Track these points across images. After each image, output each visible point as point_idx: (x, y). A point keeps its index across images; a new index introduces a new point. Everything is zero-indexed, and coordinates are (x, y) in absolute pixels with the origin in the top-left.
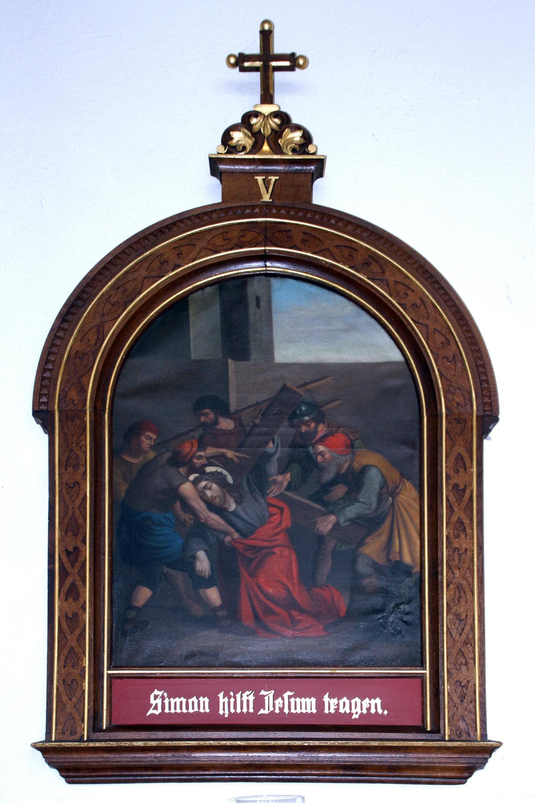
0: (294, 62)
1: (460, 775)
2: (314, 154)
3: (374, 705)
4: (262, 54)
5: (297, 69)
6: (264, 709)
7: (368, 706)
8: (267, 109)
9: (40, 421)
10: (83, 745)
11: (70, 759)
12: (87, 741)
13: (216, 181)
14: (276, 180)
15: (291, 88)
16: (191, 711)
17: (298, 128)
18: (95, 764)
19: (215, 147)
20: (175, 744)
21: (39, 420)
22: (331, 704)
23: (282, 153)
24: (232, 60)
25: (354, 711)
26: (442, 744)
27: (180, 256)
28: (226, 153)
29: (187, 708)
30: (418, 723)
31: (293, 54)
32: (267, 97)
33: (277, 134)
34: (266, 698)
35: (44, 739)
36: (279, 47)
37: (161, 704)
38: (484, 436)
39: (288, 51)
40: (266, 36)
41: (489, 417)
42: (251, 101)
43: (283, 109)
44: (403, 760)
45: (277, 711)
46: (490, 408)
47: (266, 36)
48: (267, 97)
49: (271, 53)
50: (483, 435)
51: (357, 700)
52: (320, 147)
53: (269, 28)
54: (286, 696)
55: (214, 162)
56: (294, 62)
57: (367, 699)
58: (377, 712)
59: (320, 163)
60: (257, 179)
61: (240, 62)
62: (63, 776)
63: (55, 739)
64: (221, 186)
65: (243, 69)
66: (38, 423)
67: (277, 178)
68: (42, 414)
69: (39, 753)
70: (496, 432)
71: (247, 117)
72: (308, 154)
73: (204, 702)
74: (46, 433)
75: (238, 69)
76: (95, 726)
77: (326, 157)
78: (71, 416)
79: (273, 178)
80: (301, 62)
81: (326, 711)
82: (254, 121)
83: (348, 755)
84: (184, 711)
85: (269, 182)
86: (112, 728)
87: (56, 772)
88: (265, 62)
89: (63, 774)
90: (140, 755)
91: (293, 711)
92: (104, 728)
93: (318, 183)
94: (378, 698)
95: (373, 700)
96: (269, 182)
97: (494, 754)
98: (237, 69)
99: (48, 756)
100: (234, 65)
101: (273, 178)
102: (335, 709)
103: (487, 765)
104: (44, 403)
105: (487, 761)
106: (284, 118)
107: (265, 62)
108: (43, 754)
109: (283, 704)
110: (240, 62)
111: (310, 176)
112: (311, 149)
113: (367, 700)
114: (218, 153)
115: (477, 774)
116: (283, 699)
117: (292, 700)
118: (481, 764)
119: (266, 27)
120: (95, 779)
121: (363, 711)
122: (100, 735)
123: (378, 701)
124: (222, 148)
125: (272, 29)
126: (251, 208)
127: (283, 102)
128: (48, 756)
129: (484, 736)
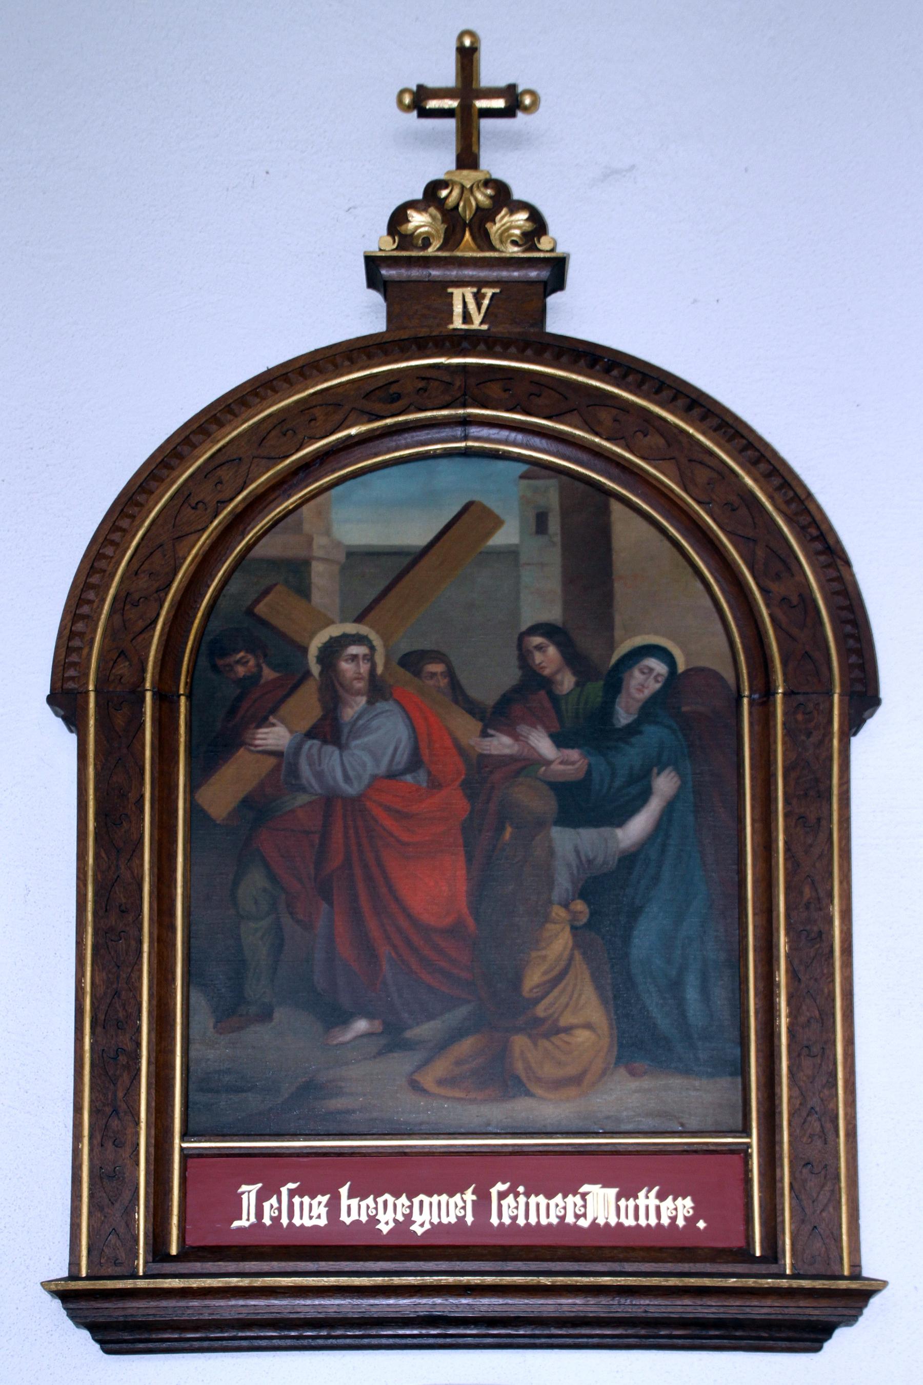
0: (515, 102)
1: (809, 1335)
2: (552, 250)
3: (663, 1210)
4: (460, 86)
5: (520, 114)
6: (240, 1218)
7: (408, 1211)
8: (468, 177)
9: (62, 713)
10: (784, 1283)
11: (107, 1310)
12: (88, 1278)
13: (376, 298)
14: (494, 294)
15: (516, 141)
16: (643, 1222)
17: (524, 206)
18: (572, 1315)
19: (379, 241)
20: (226, 1282)
21: (57, 709)
22: (354, 1210)
23: (493, 248)
24: (407, 99)
25: (416, 1216)
26: (129, 1284)
27: (313, 423)
28: (396, 249)
29: (637, 1217)
30: (737, 1242)
31: (512, 88)
32: (467, 158)
33: (485, 215)
34: (245, 1197)
35: (65, 1273)
36: (490, 74)
37: (254, 1208)
38: (854, 730)
39: (502, 83)
40: (467, 57)
41: (864, 698)
42: (442, 163)
43: (495, 176)
44: (689, 1309)
45: (267, 1221)
46: (861, 675)
47: (467, 57)
48: (467, 158)
49: (474, 86)
50: (850, 729)
51: (541, 1199)
52: (561, 237)
53: (472, 43)
54: (284, 1190)
55: (372, 263)
56: (515, 102)
57: (670, 1198)
58: (538, 1223)
59: (557, 269)
60: (452, 294)
61: (419, 101)
62: (97, 1341)
63: (144, 1272)
64: (384, 304)
65: (425, 113)
66: (57, 714)
67: (497, 290)
68: (64, 700)
69: (57, 1304)
70: (872, 725)
71: (433, 188)
72: (539, 250)
73: (538, 1205)
74: (71, 731)
75: (415, 113)
76: (158, 1251)
77: (569, 255)
78: (119, 703)
79: (489, 292)
80: (527, 101)
81: (495, 1221)
82: (444, 193)
83: (501, 1301)
84: (533, 1220)
85: (465, 311)
86: (186, 1254)
87: (85, 1334)
88: (467, 102)
89: (100, 1337)
90: (647, 1302)
91: (297, 1221)
92: (758, 1254)
93: (553, 300)
94: (689, 1198)
95: (631, 1200)
96: (465, 311)
97: (875, 1301)
98: (415, 113)
99: (71, 1306)
100: (408, 109)
101: (489, 292)
102: (670, 1218)
103: (861, 1319)
104: (72, 678)
105: (861, 1314)
106: (502, 195)
107: (467, 102)
108: (63, 1302)
109: (279, 1209)
110: (419, 101)
111: (540, 289)
112: (544, 243)
113: (559, 1198)
114: (380, 250)
115: (840, 1334)
116: (279, 1201)
117: (297, 1200)
118: (851, 1319)
119: (467, 42)
120: (151, 1345)
121: (662, 1222)
122: (168, 1267)
123: (688, 1202)
124: (390, 239)
125: (475, 45)
126: (640, 376)
127: (494, 162)
128: (71, 1306)
129: (856, 1265)
